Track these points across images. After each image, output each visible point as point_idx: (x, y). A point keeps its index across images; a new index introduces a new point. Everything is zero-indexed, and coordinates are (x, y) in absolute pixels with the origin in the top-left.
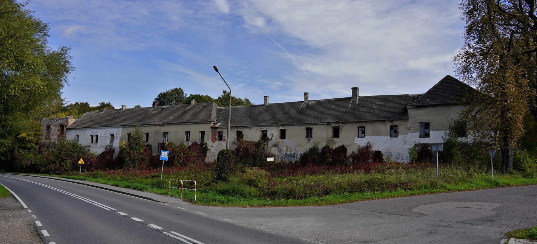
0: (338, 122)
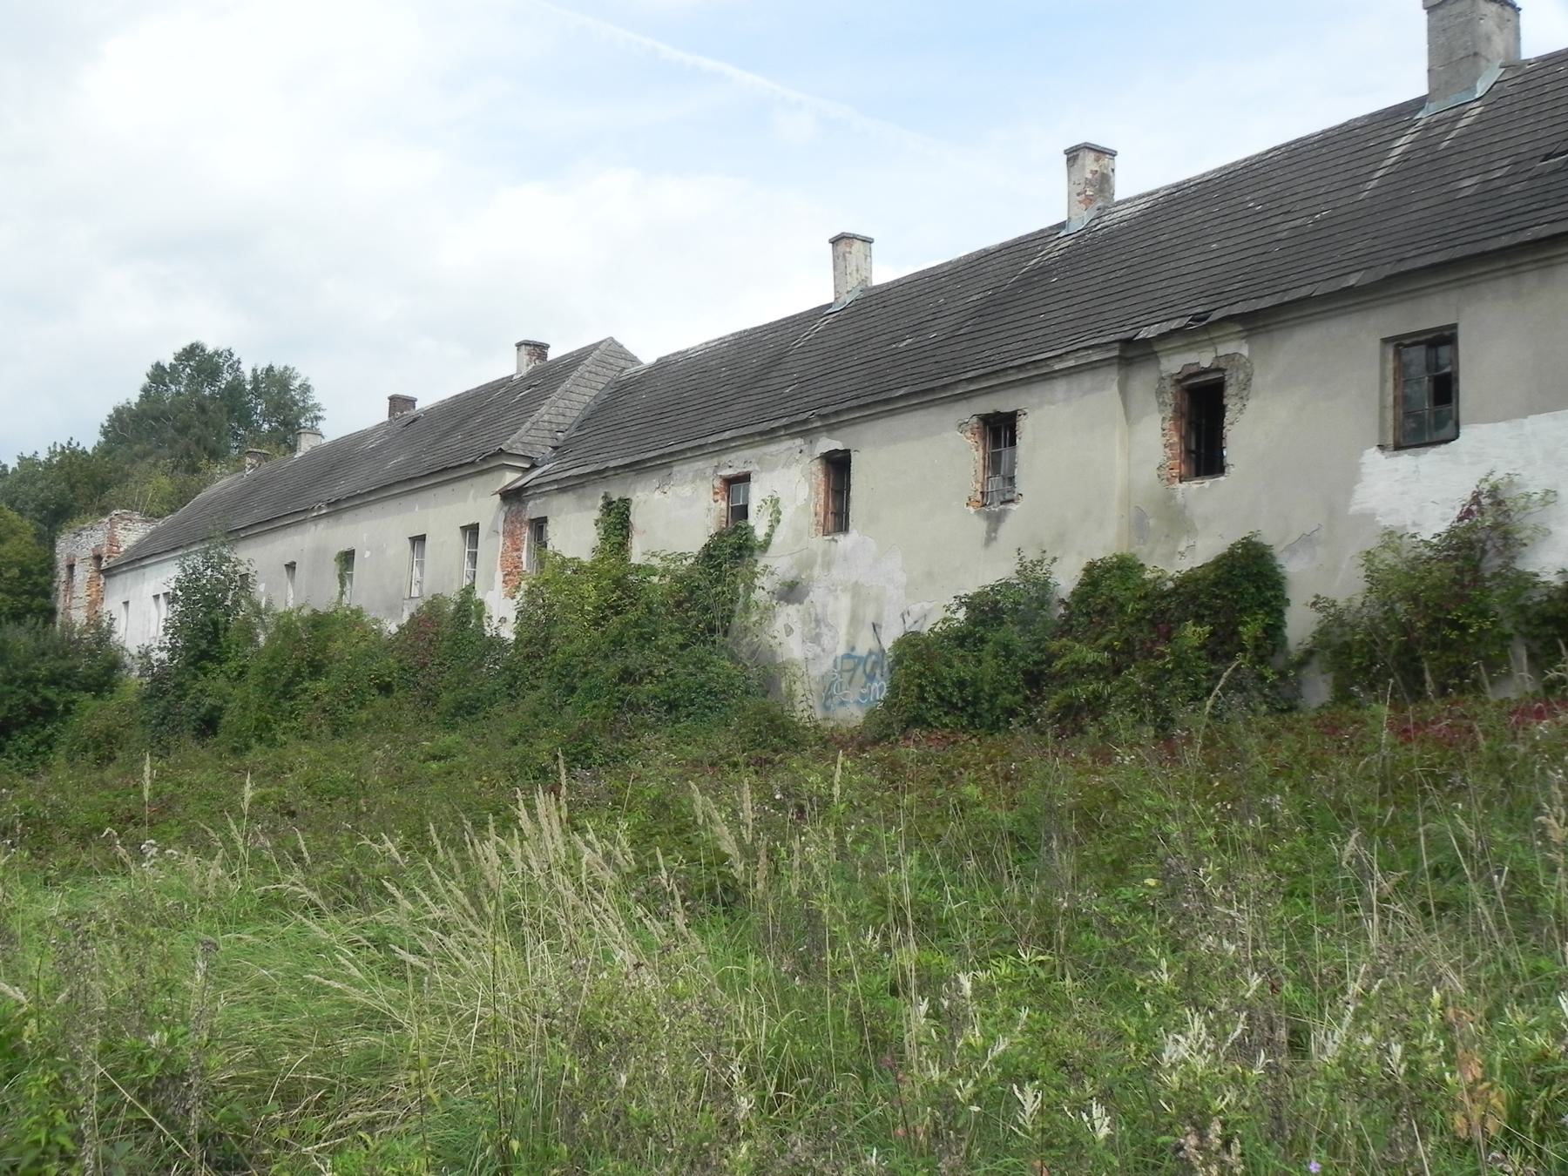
0: (1201, 328)
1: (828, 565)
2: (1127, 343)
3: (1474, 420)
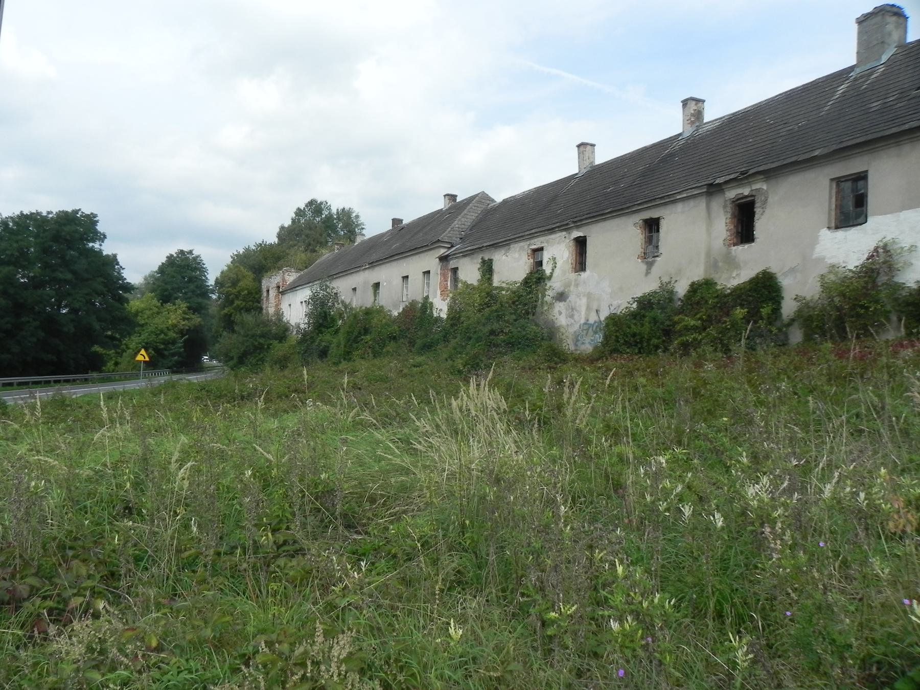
0: (744, 178)
1: (577, 285)
2: (711, 185)
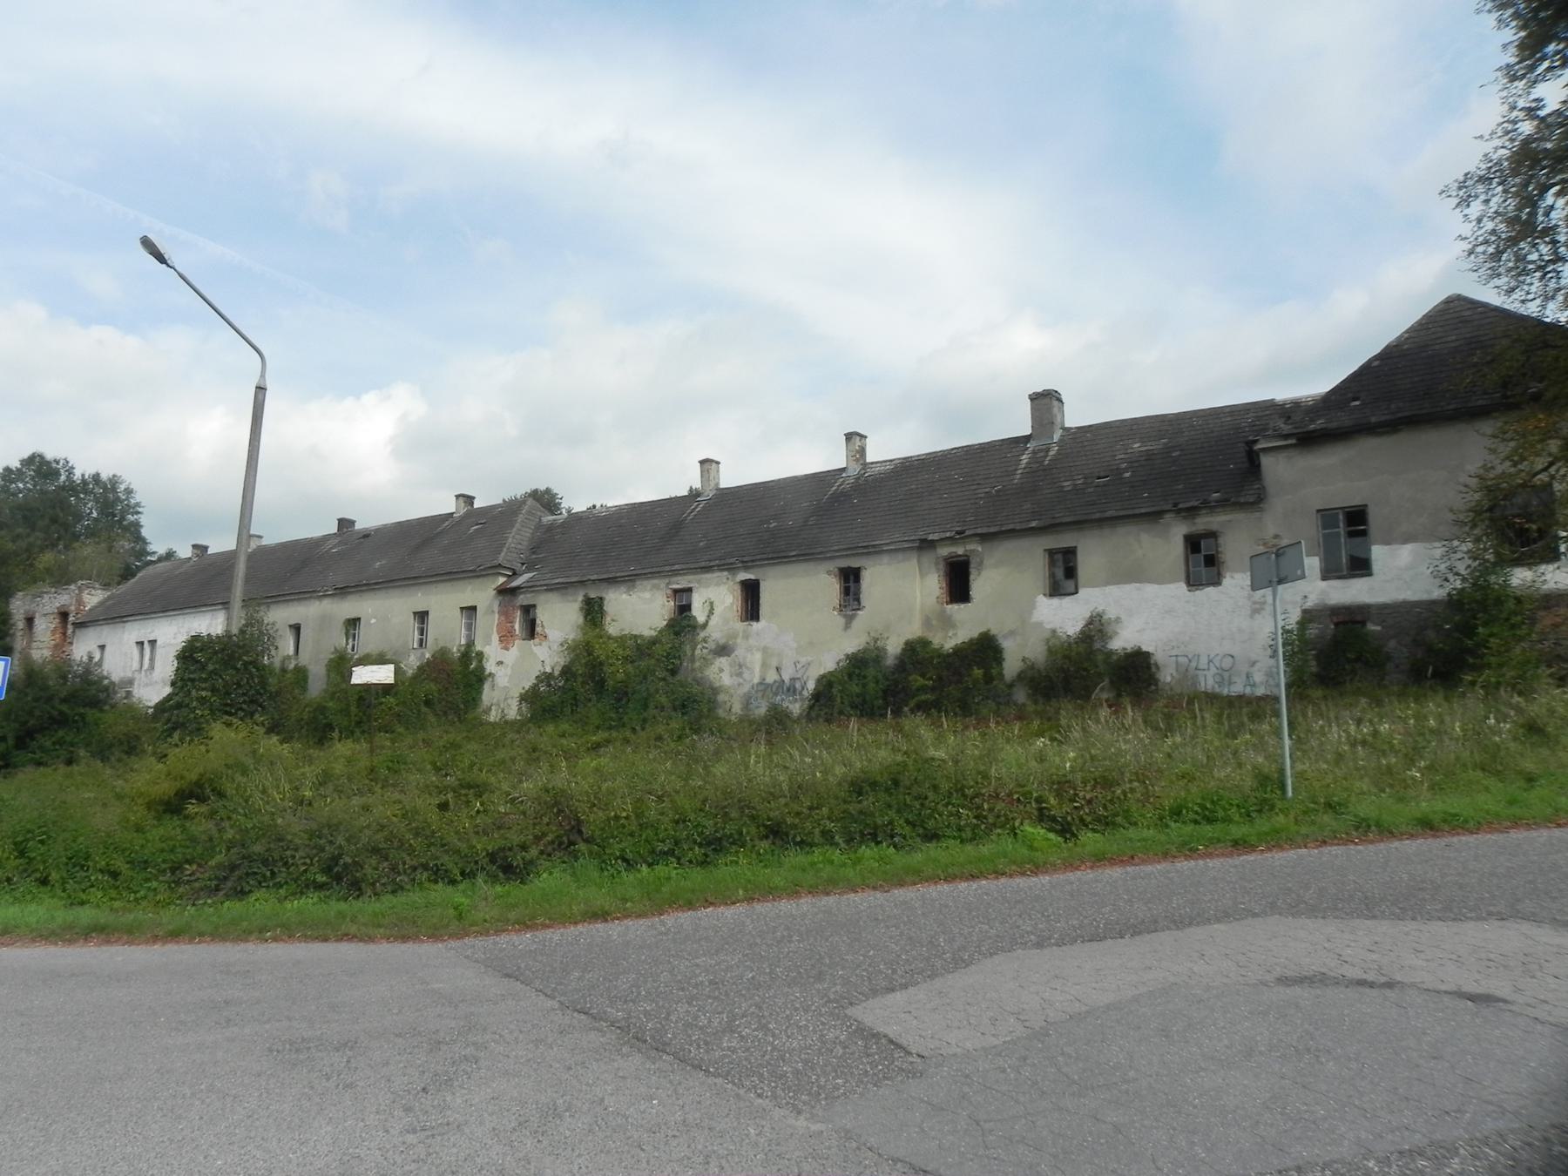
0: (960, 537)
1: (746, 637)
2: (923, 541)
3: (1093, 584)
